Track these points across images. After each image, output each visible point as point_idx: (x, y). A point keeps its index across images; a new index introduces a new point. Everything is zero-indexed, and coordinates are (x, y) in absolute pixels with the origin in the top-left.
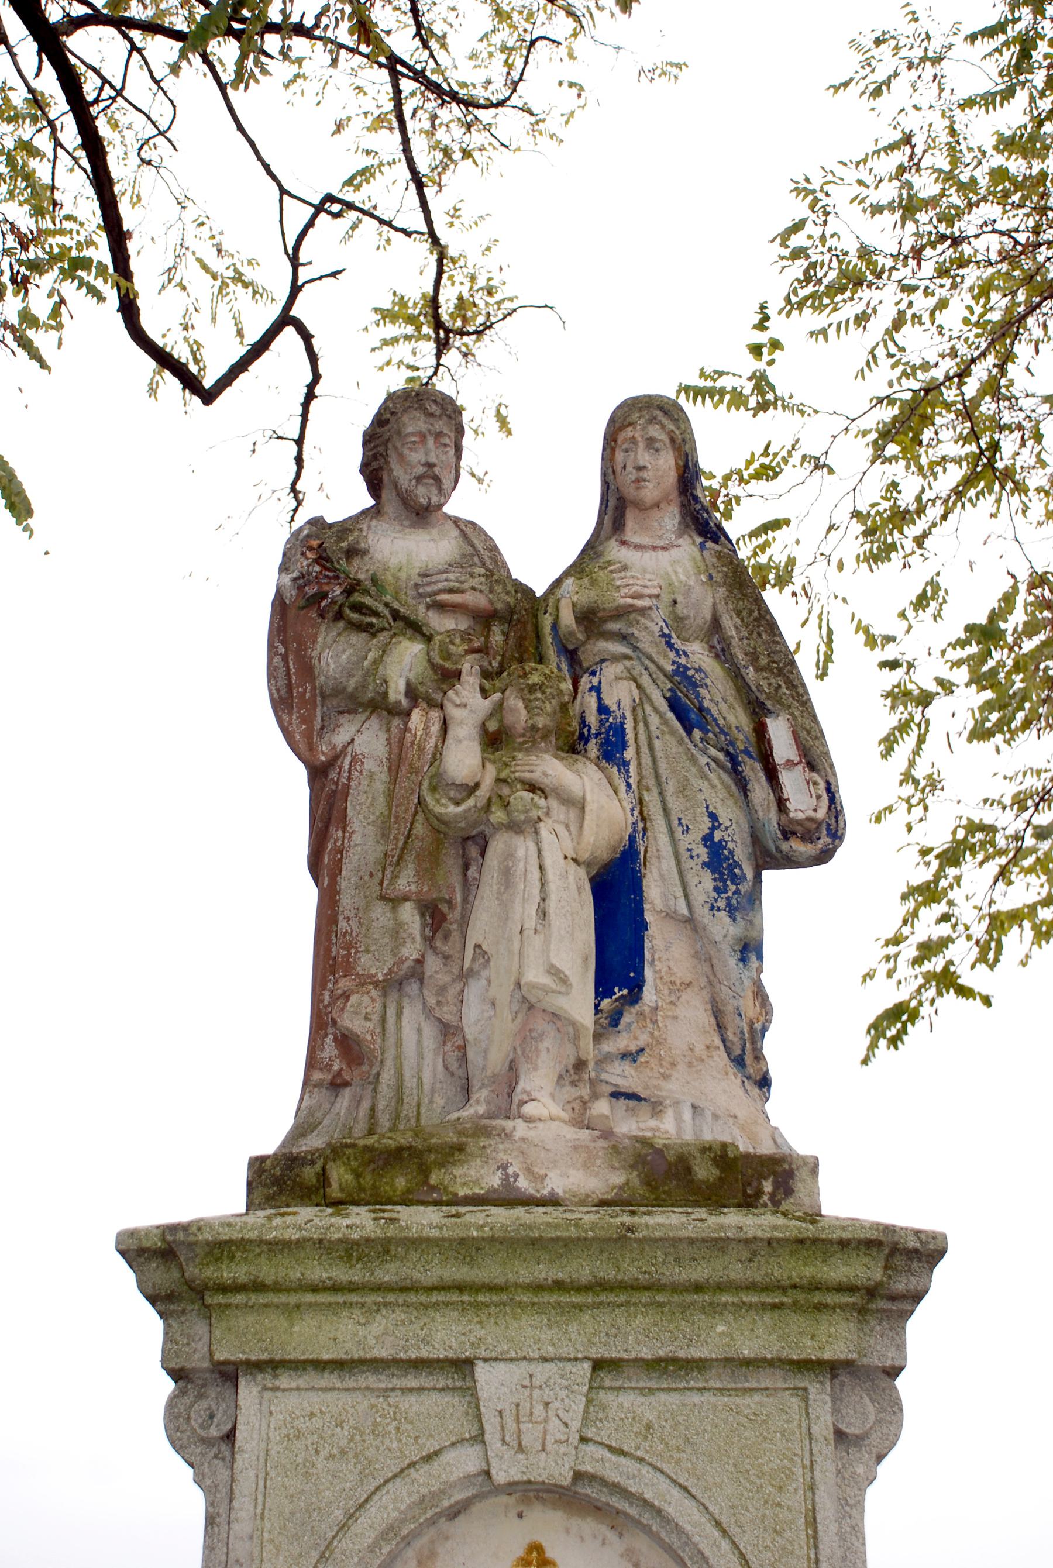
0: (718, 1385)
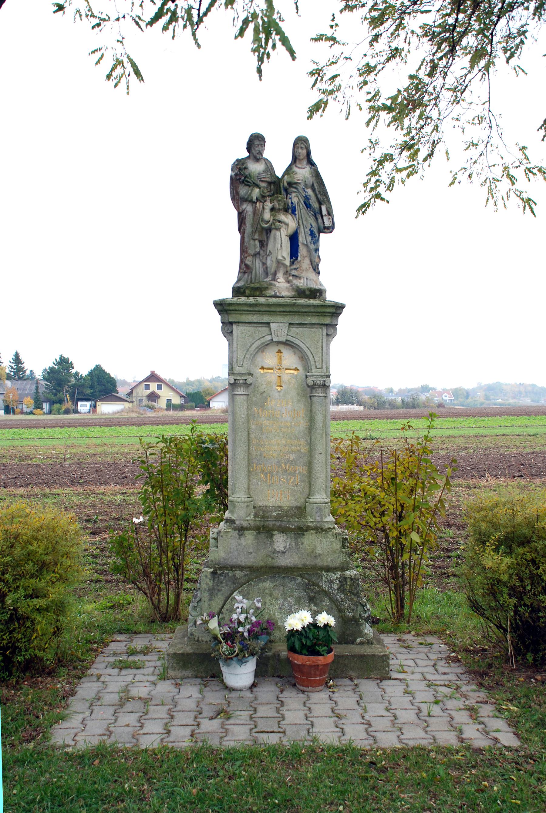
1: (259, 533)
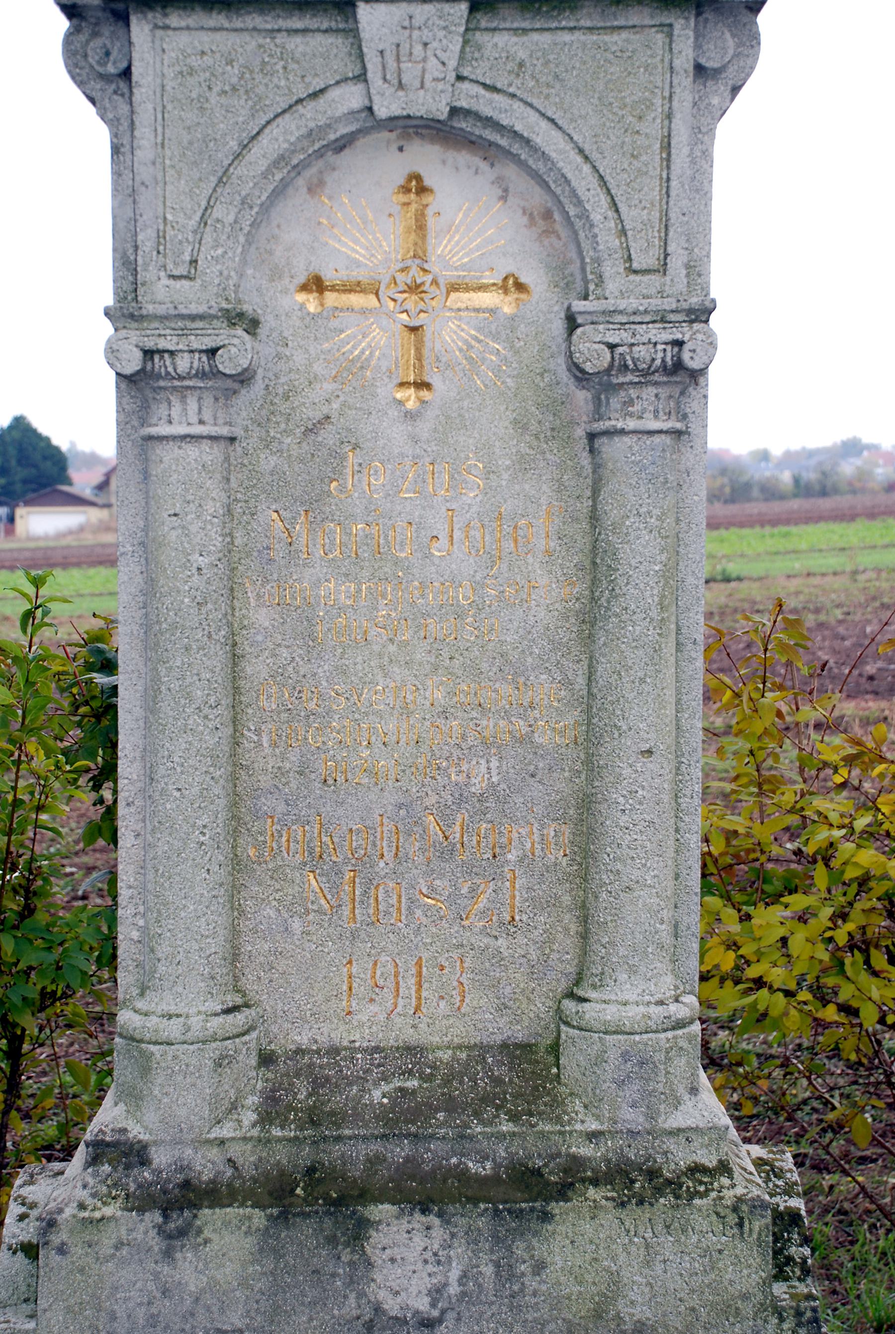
0: (589, 24)
1: (284, 1217)
